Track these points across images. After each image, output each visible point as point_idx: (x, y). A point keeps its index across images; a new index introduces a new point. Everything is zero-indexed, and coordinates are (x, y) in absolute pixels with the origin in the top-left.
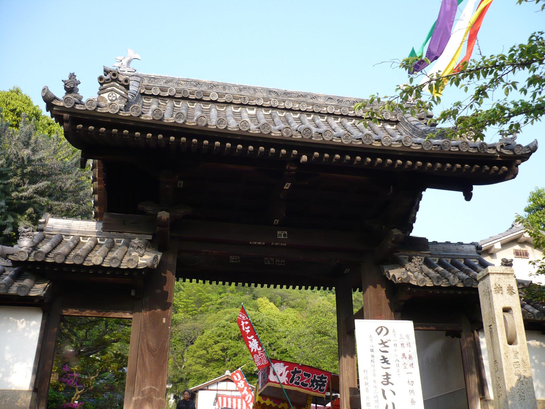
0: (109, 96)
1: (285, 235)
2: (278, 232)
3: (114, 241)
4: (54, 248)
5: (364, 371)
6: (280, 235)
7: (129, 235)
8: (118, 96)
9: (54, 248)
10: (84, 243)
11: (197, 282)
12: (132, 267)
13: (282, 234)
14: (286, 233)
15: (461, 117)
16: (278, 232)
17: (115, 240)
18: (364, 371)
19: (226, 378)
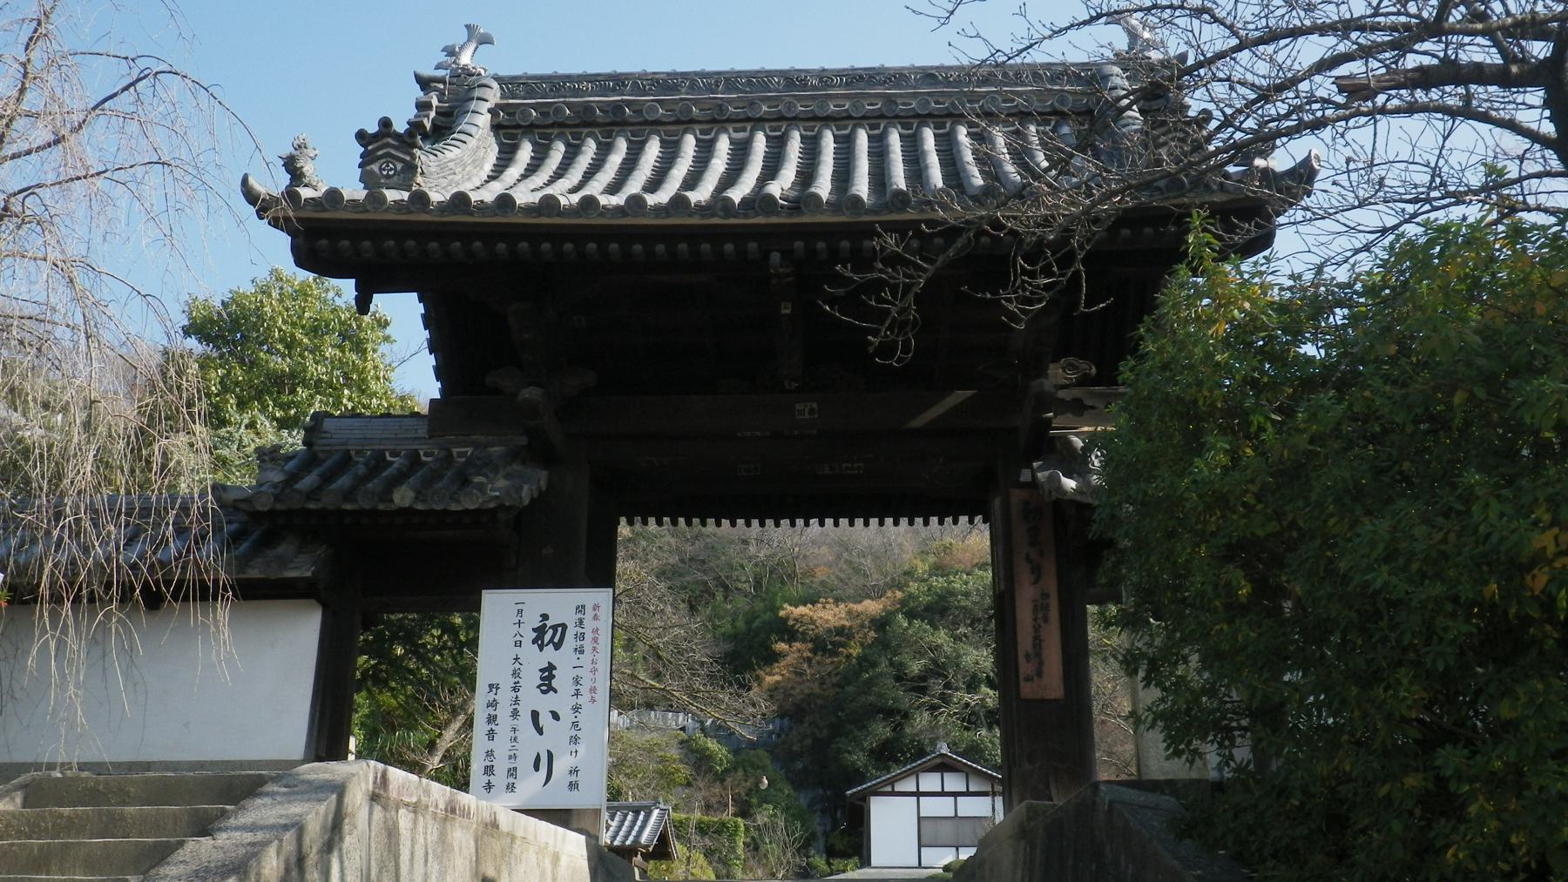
0: (381, 169)
1: (812, 411)
2: (798, 407)
3: (451, 454)
4: (327, 479)
5: (491, 686)
6: (802, 412)
7: (482, 439)
8: (399, 166)
9: (327, 479)
10: (392, 463)
11: (836, 524)
12: (472, 507)
13: (805, 409)
14: (815, 405)
15: (301, 261)
16: (798, 407)
17: (455, 451)
18: (491, 686)
19: (938, 761)
